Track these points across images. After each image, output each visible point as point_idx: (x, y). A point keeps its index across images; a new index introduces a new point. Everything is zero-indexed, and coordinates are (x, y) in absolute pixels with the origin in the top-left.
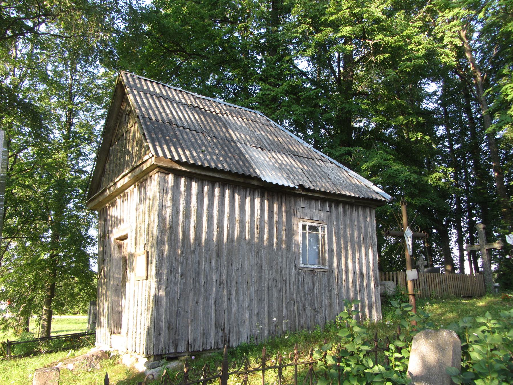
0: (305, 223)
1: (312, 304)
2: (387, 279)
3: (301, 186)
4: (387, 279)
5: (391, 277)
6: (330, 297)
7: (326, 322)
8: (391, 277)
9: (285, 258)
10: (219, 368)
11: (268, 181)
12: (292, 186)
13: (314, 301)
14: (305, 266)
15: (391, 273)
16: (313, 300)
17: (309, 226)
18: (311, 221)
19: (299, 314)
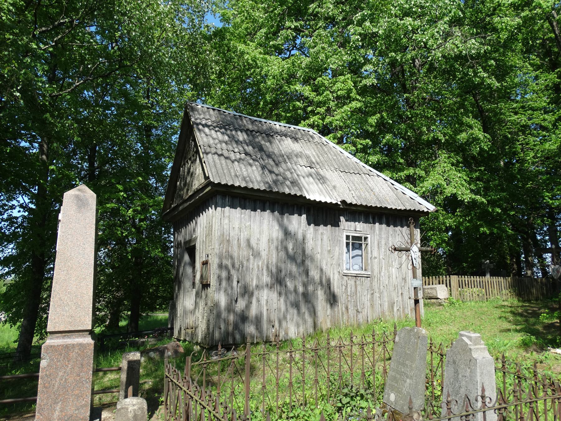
0: (348, 234)
1: (356, 306)
2: (431, 283)
3: (343, 202)
4: (431, 283)
5: (445, 281)
6: (372, 299)
7: (368, 321)
8: (445, 281)
9: (329, 265)
10: (96, 13)
11: (312, 199)
12: (334, 202)
13: (357, 303)
14: (348, 272)
15: (441, 277)
16: (356, 302)
17: (192, 362)
18: (355, 232)
19: (343, 314)
